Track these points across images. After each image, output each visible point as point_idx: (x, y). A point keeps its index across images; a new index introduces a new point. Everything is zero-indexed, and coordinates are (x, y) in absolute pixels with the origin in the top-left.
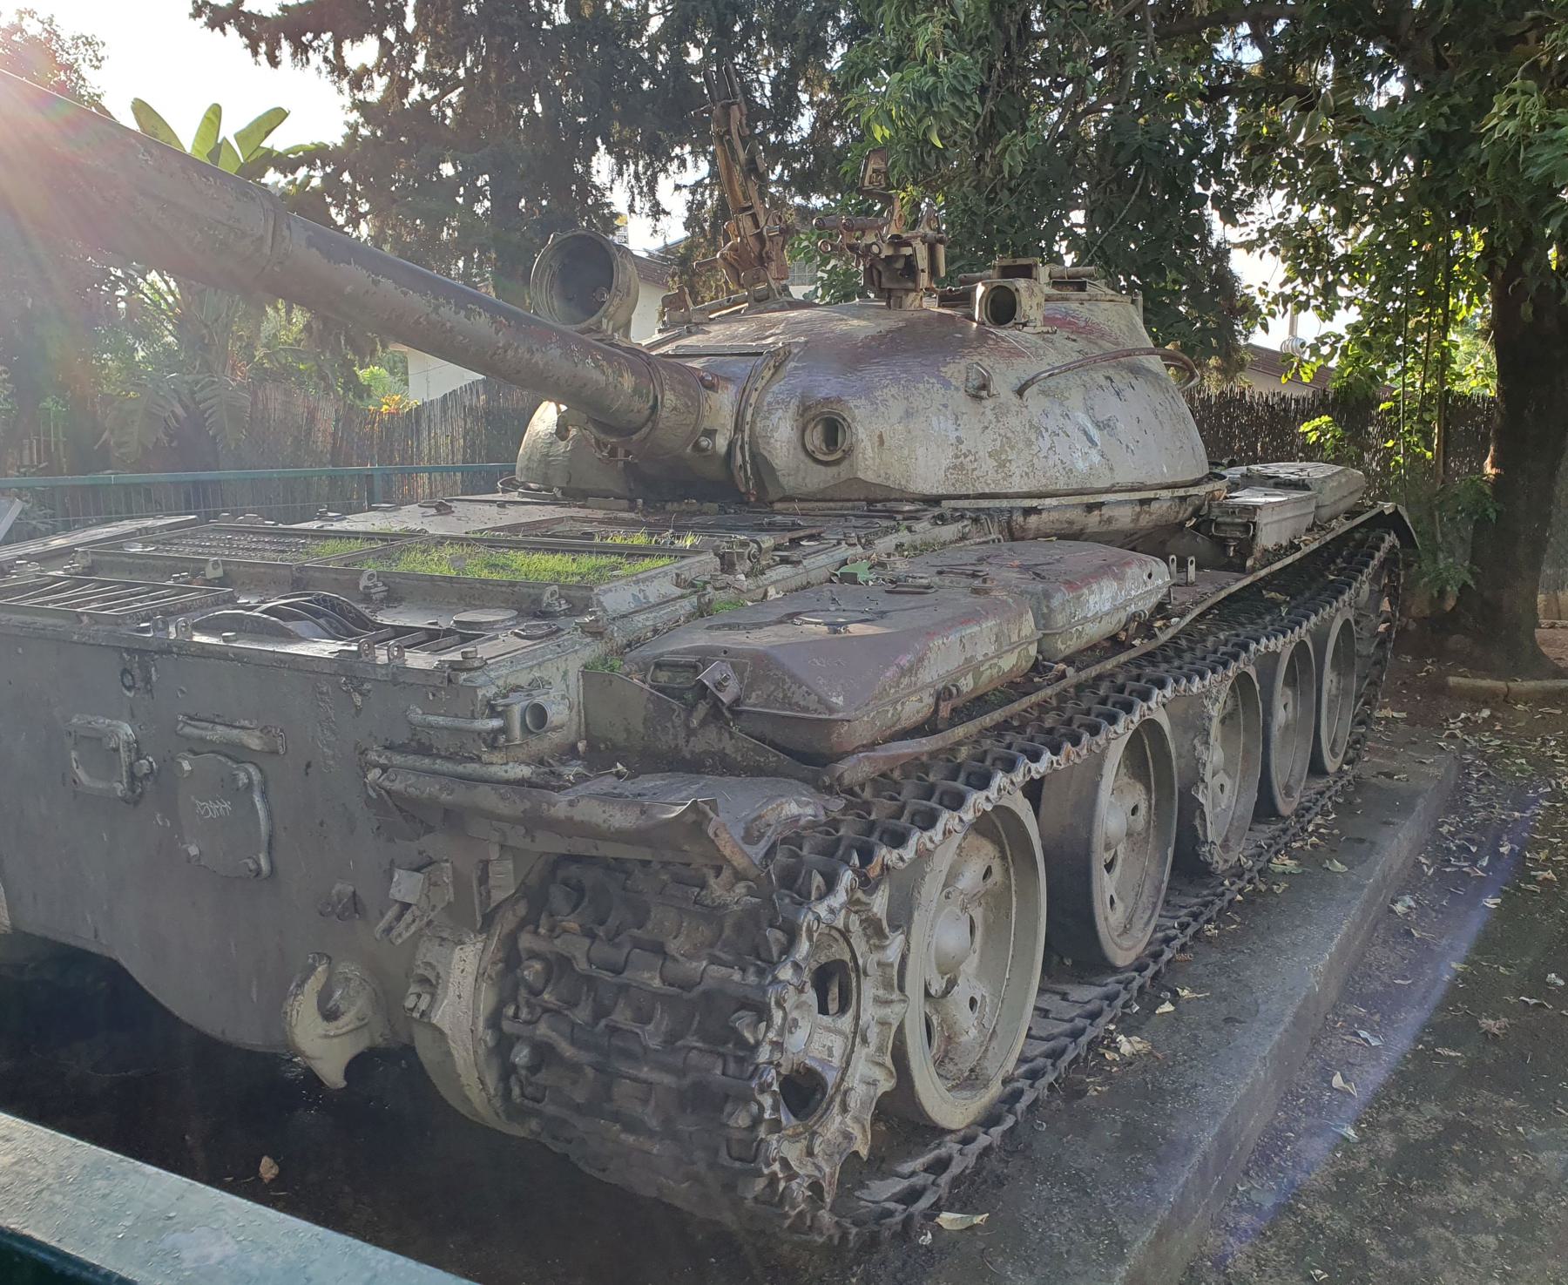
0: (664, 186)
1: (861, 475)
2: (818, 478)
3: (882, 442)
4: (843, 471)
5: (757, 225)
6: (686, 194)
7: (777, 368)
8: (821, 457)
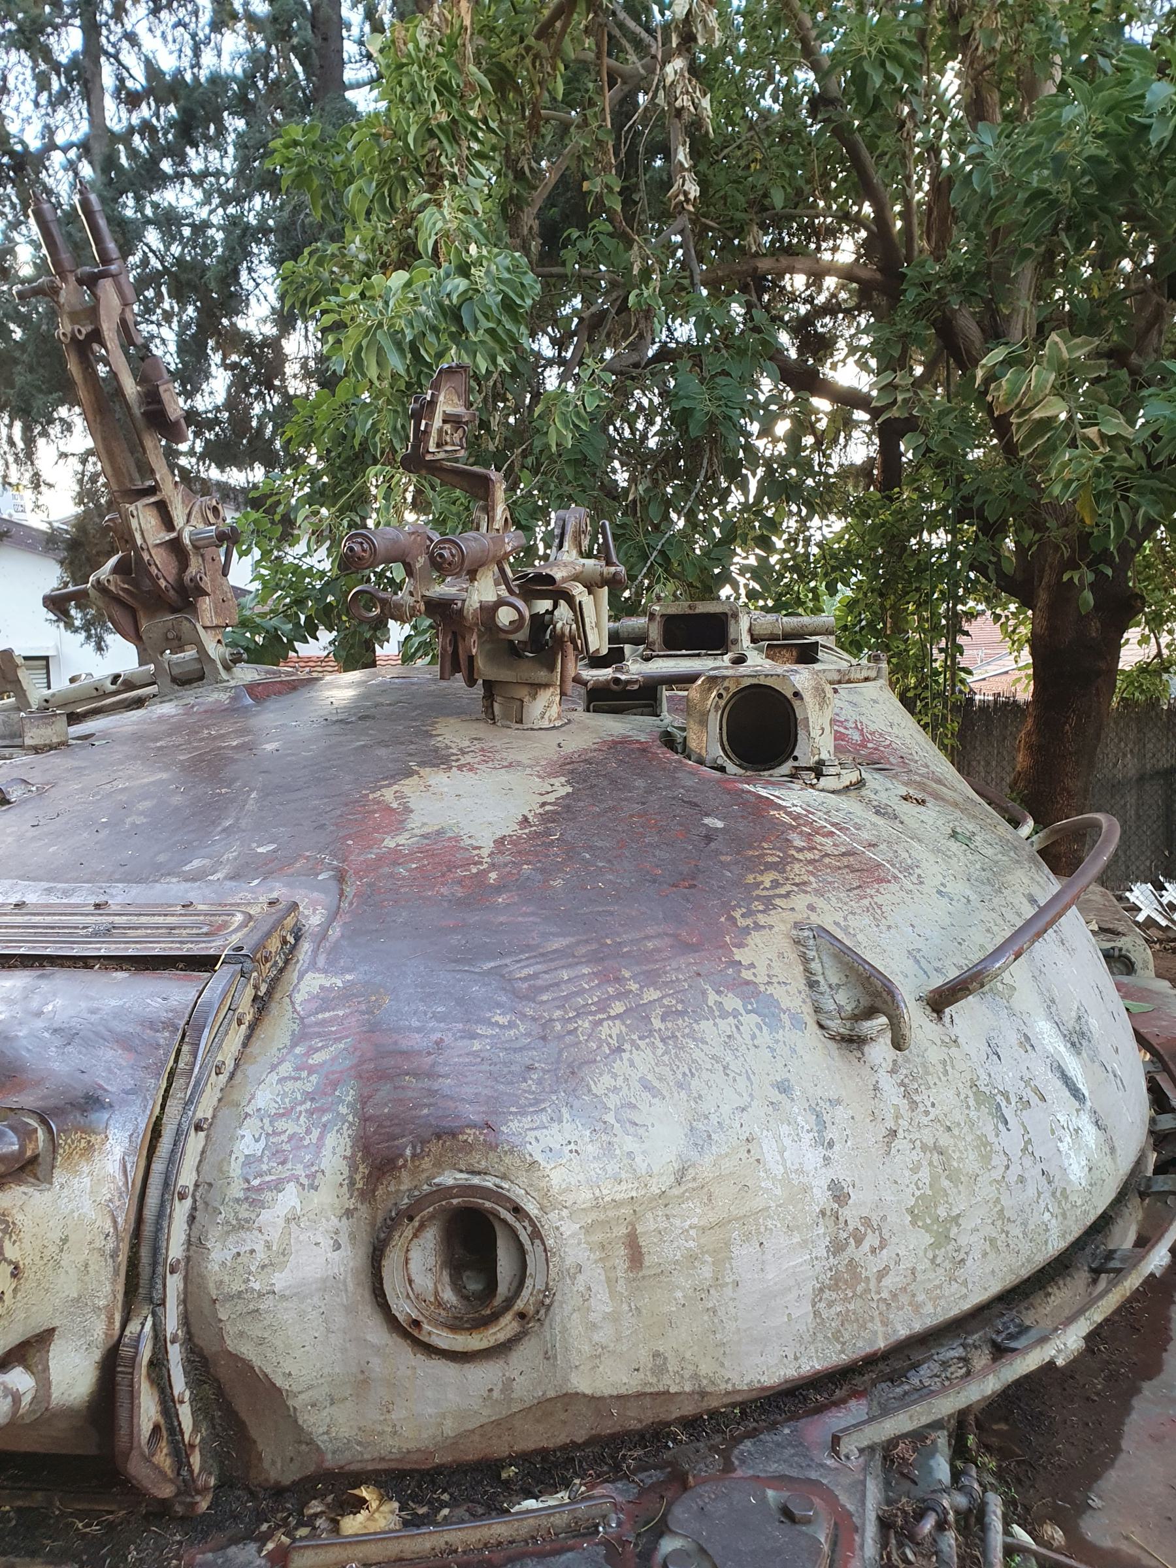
0: (45, 451)
1: (582, 1383)
2: (440, 1403)
3: (636, 1256)
4: (522, 1376)
5: (168, 522)
6: (74, 464)
7: (262, 1004)
8: (443, 1339)
